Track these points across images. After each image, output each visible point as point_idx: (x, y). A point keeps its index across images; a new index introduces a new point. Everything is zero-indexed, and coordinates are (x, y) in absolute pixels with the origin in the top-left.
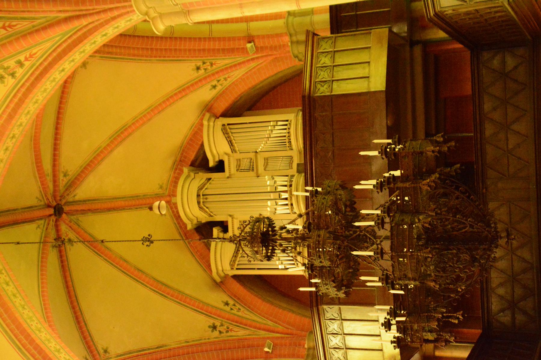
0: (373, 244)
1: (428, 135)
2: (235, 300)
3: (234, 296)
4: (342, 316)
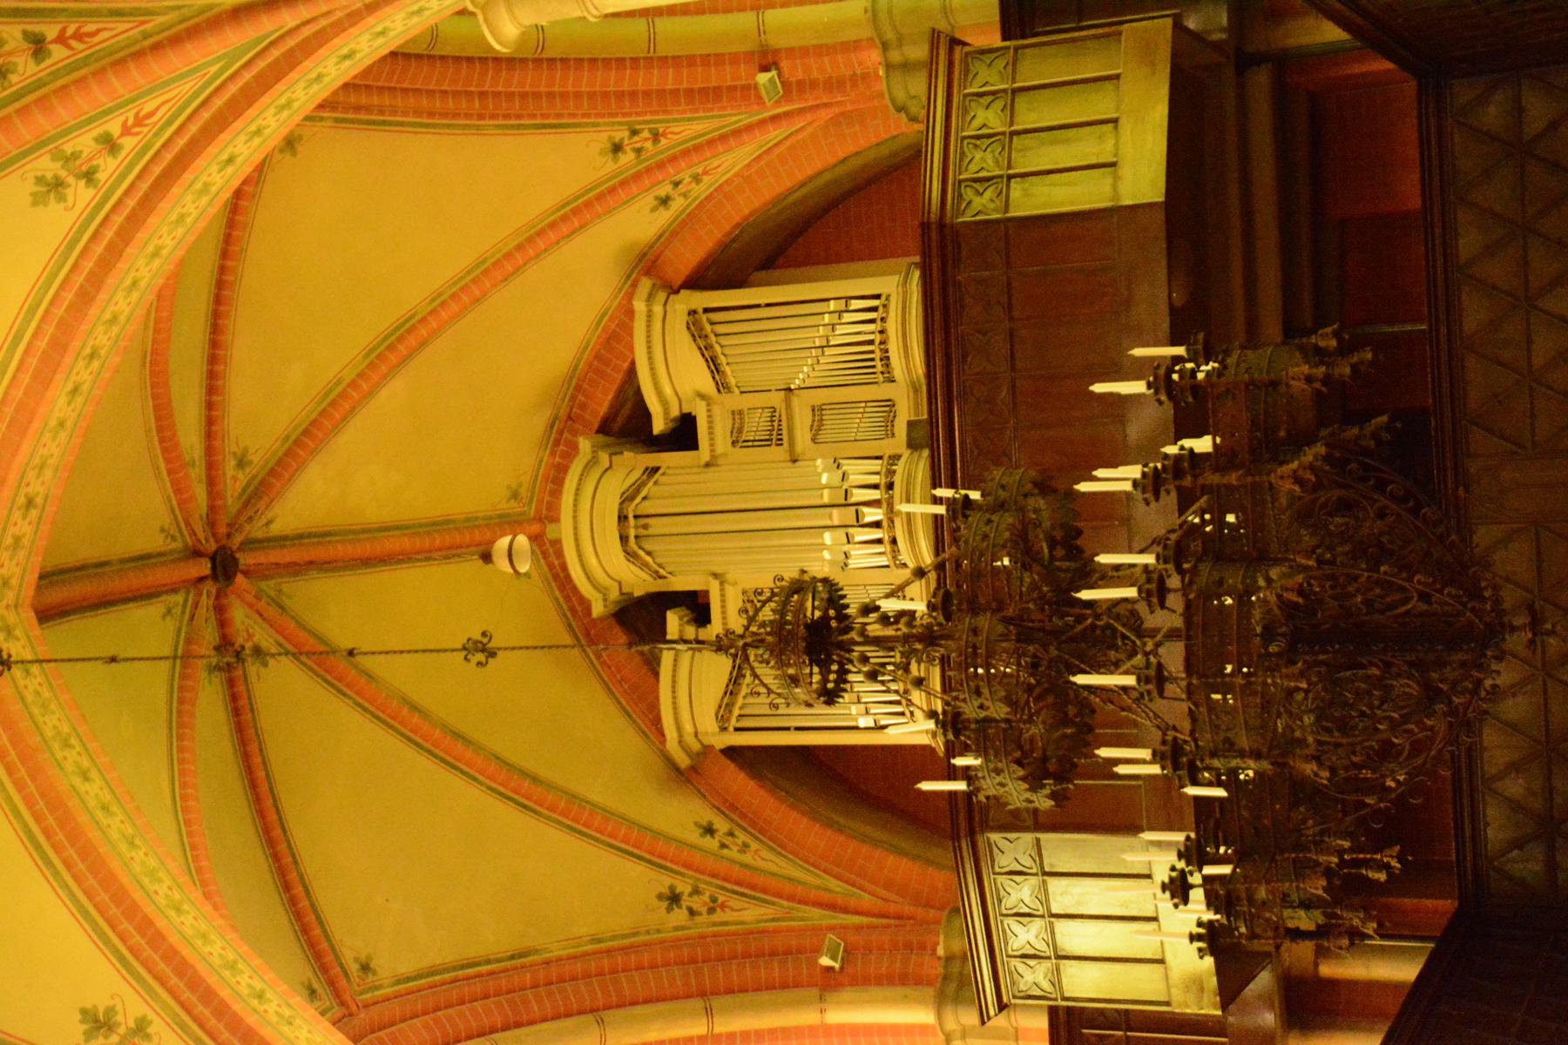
1: (1291, 330)
2: (732, 820)
3: (729, 807)
4: (1045, 862)
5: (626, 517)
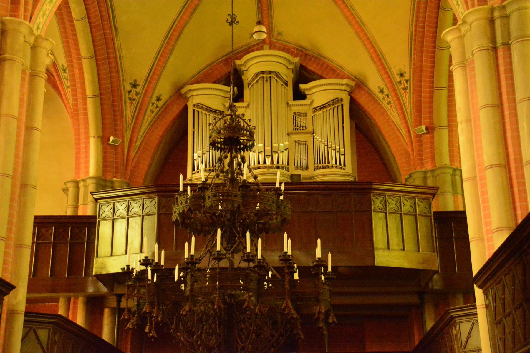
0: (225, 249)
1: (335, 307)
2: (162, 107)
3: (167, 107)
4: (147, 217)
5: (270, 74)
